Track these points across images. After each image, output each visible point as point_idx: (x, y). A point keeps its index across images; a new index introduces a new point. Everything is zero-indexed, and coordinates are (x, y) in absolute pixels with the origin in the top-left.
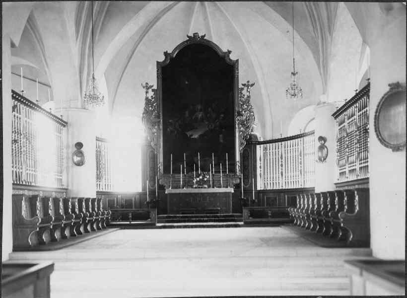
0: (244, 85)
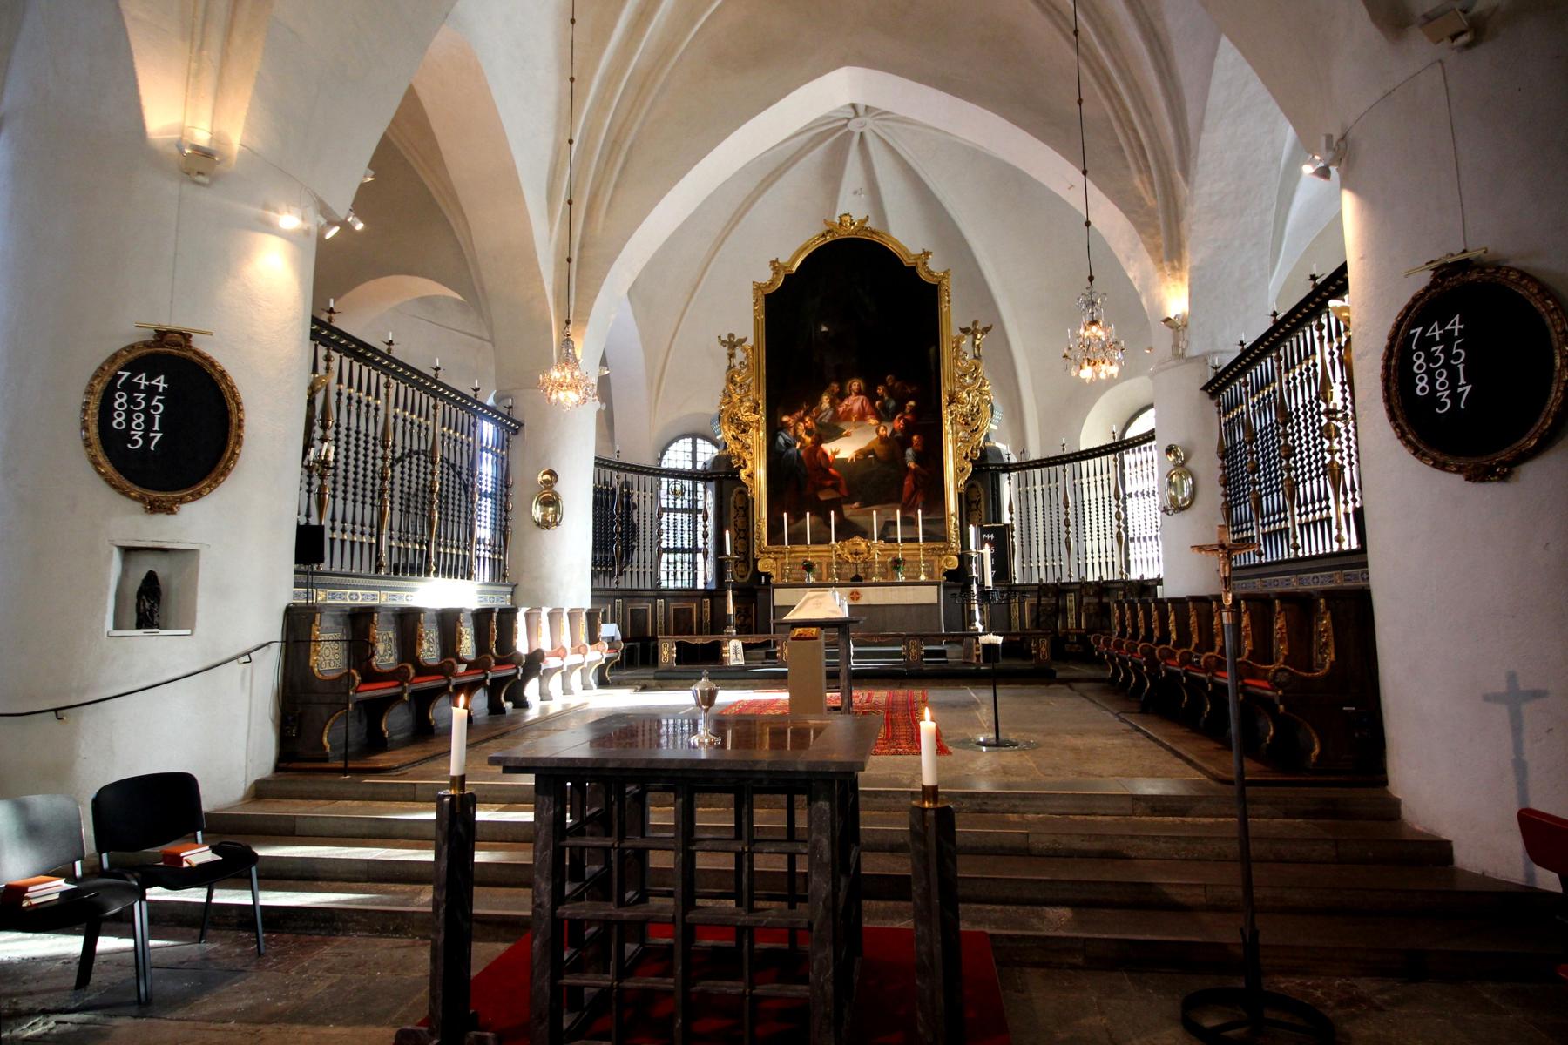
0: (965, 331)
